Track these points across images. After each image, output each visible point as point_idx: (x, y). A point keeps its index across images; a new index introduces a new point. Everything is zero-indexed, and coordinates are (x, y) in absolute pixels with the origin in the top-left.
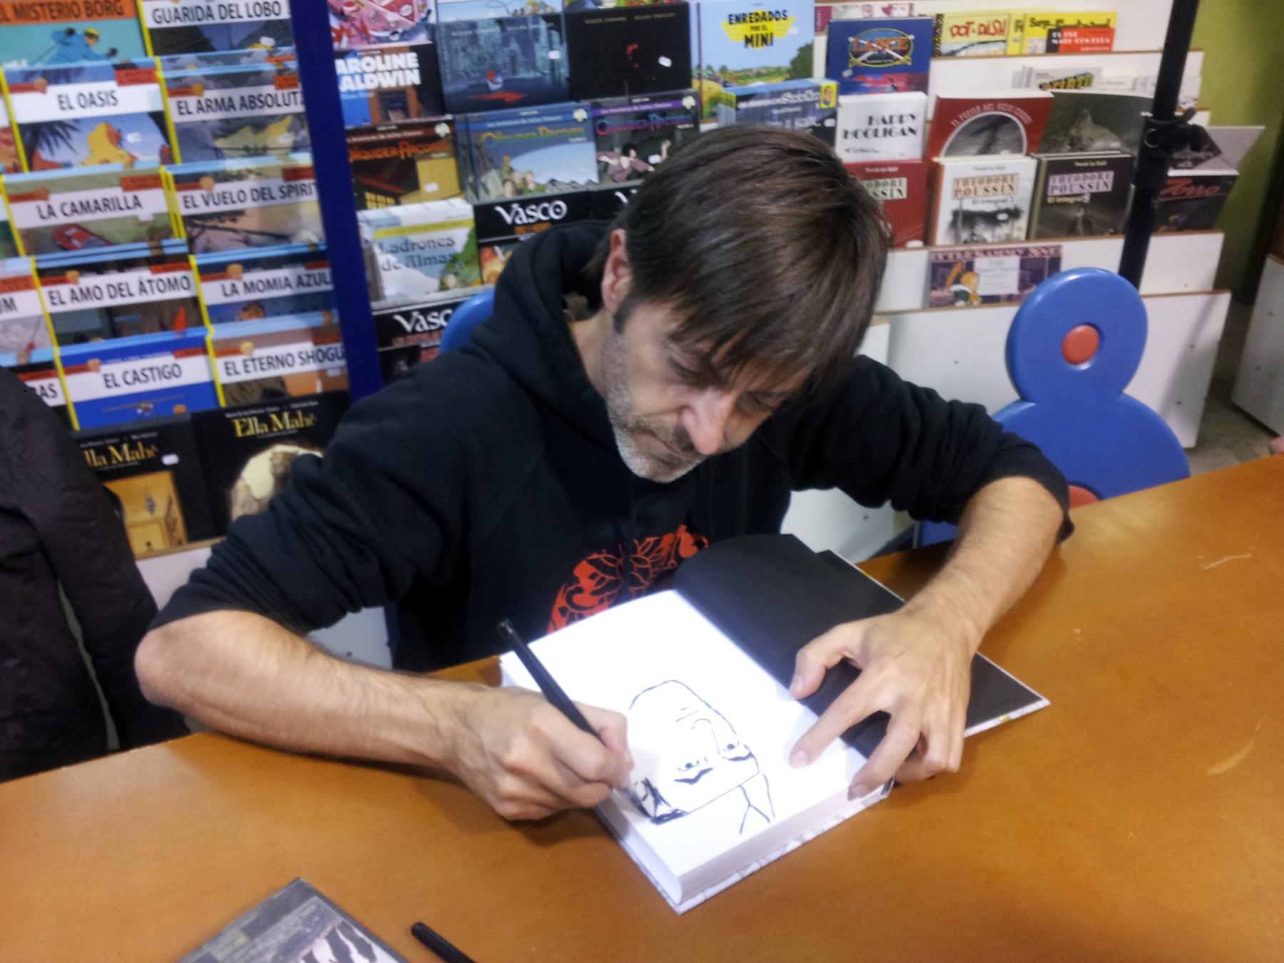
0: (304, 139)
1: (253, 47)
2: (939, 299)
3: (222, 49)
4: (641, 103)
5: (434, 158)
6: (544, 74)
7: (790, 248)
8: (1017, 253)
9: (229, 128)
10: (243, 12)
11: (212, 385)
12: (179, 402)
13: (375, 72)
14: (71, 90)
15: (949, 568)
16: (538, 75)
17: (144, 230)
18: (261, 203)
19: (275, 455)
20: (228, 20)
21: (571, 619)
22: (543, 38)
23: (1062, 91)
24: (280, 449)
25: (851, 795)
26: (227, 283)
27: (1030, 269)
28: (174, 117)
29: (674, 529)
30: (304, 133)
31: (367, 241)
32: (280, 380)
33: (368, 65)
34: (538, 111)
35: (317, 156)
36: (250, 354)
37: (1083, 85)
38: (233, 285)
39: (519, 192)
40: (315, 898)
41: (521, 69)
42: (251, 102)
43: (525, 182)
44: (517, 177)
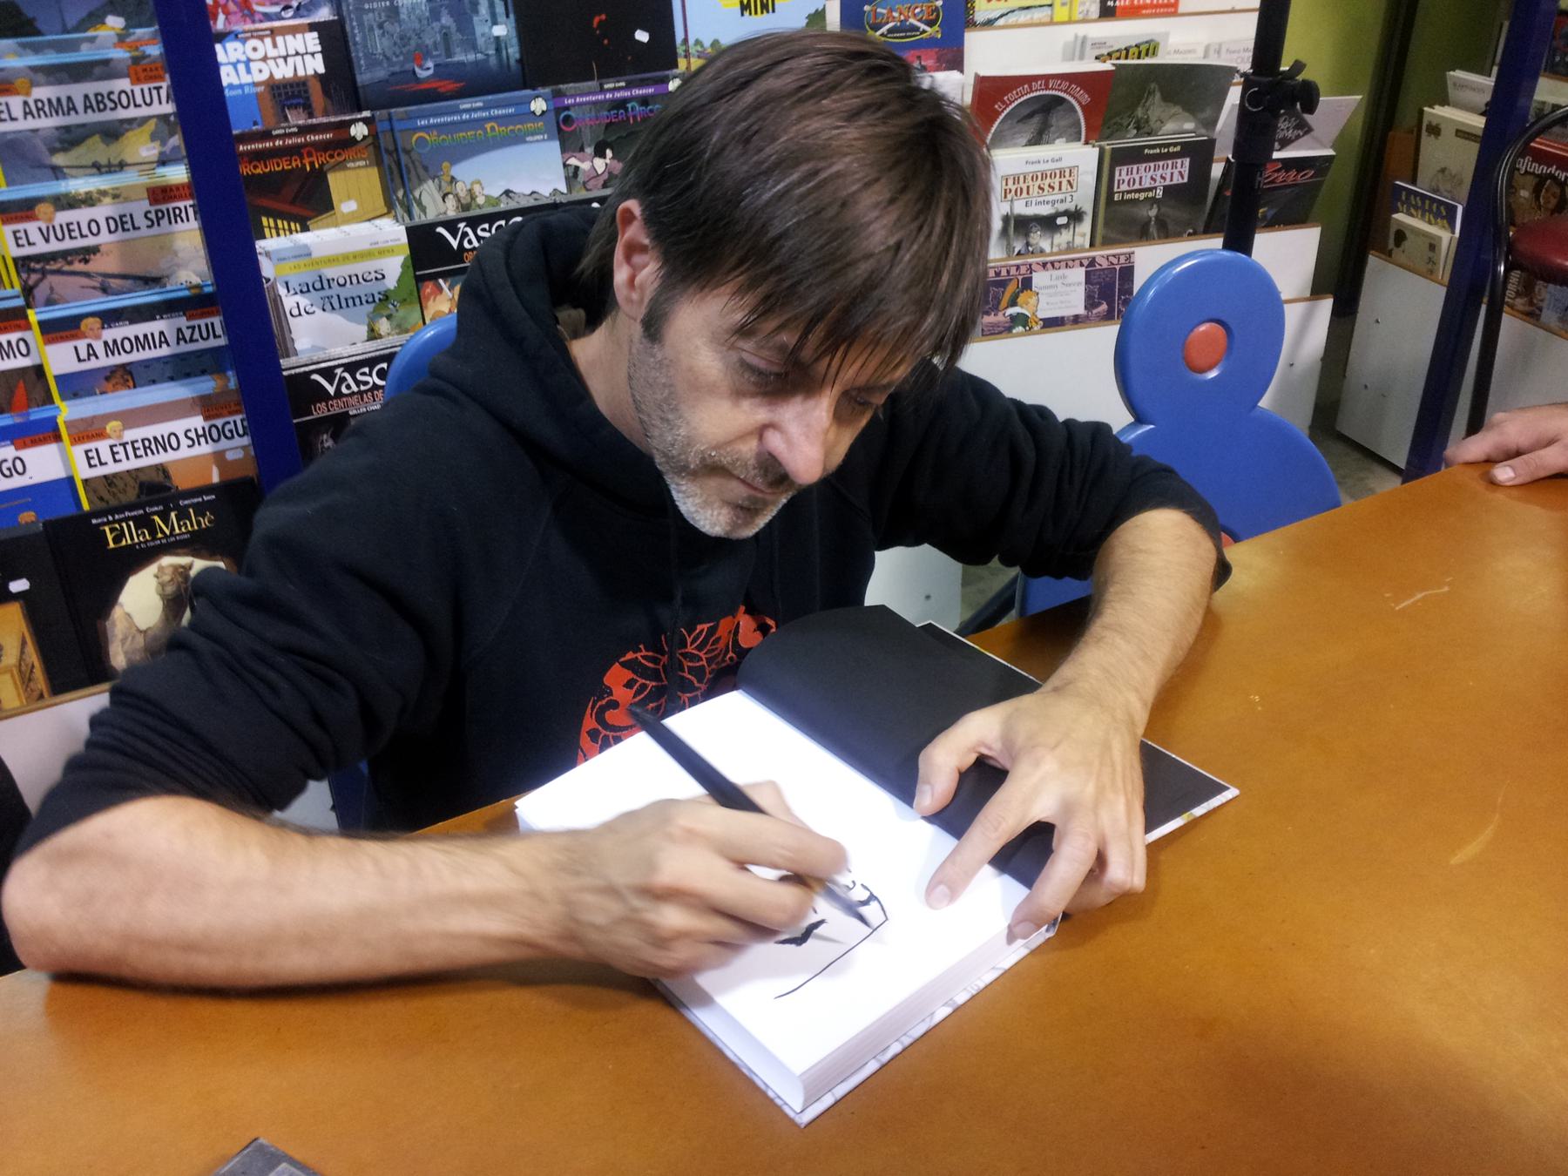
0: (175, 149)
1: (96, 30)
2: (994, 325)
3: (51, 33)
4: (616, 89)
5: (350, 169)
6: (487, 55)
7: (883, 181)
8: (1082, 265)
9: (70, 138)
11: (70, 480)
12: (27, 507)
13: (265, 59)
15: (1097, 628)
16: (480, 56)
18: (120, 235)
19: (161, 569)
21: (605, 745)
23: (1122, 62)
24: (167, 561)
25: (1011, 937)
26: (82, 344)
27: (1099, 283)
29: (732, 612)
30: (176, 140)
31: (268, 280)
32: (162, 469)
33: (255, 49)
34: (484, 102)
35: (194, 169)
36: (120, 437)
37: (1147, 55)
38: (90, 346)
39: (466, 208)
40: (284, 1165)
41: (458, 50)
42: (98, 103)
44: (461, 189)
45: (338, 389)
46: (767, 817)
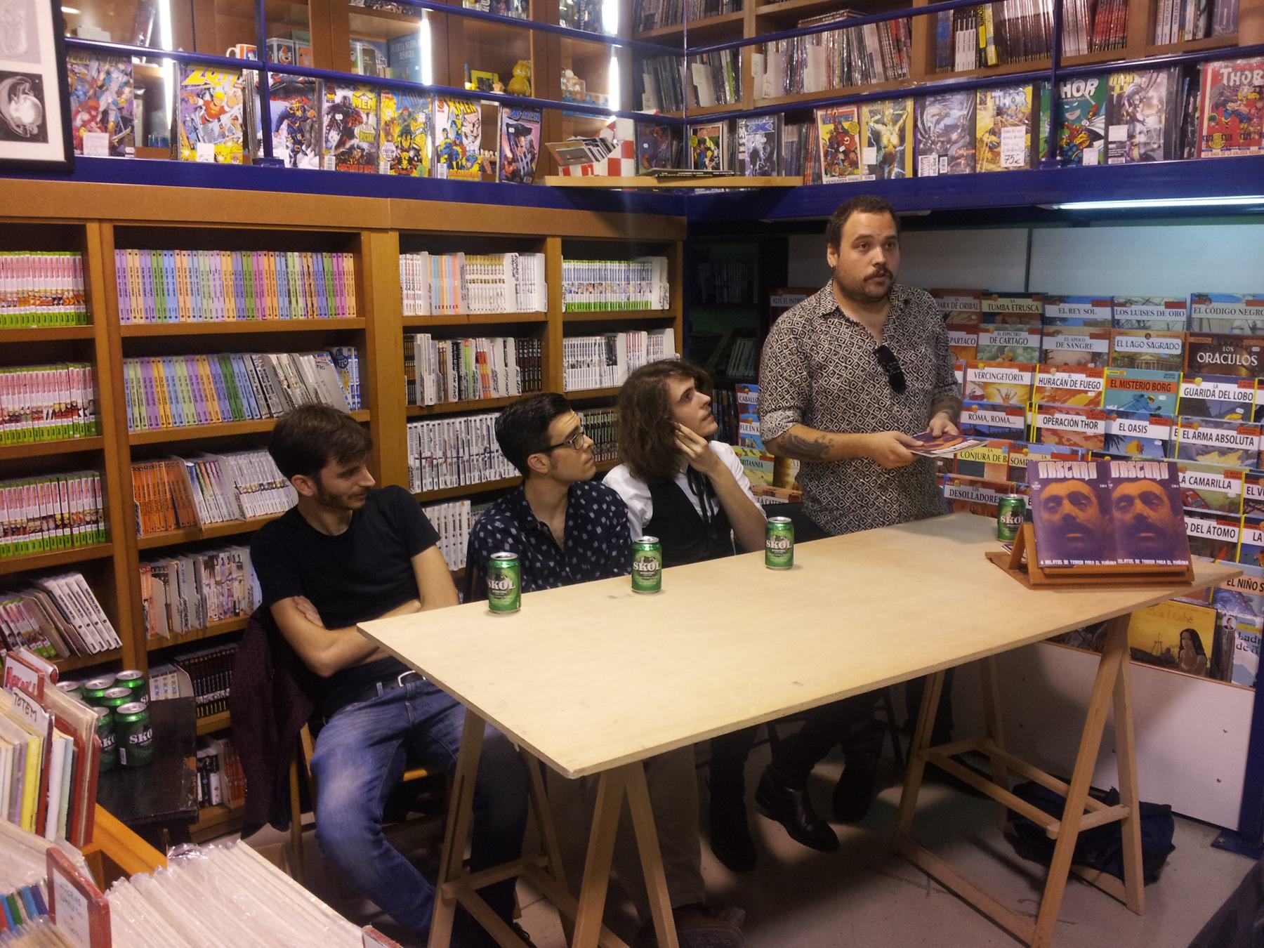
14: (1126, 422)
17: (1228, 501)
20: (1222, 399)
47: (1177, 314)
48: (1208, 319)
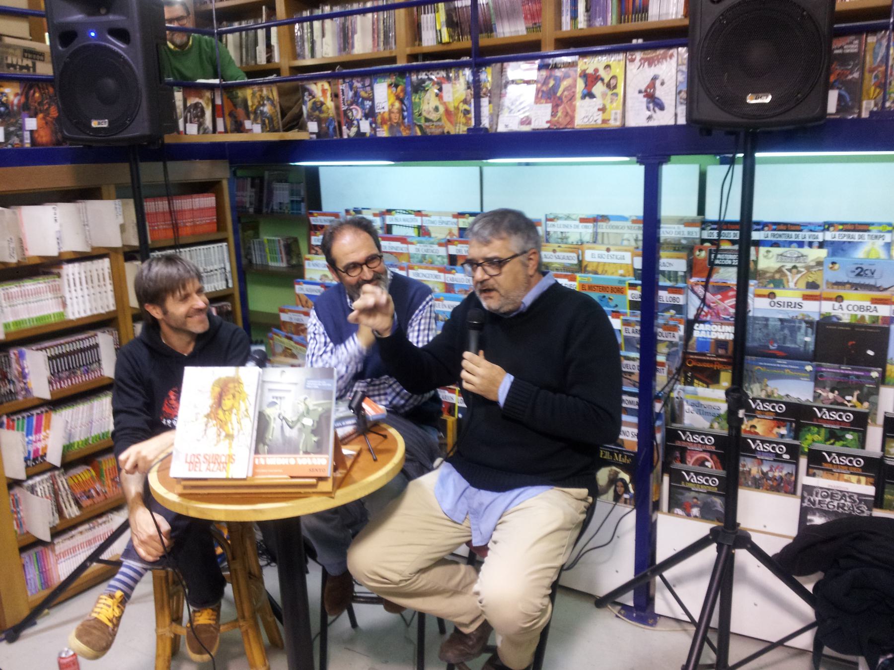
4: (845, 369)
10: (665, 299)
16: (797, 346)
22: (803, 331)
24: (614, 468)
28: (624, 333)
39: (769, 396)
43: (773, 392)
44: (769, 389)
45: (831, 461)
46: (551, 623)
47: (586, 227)
48: (608, 233)
